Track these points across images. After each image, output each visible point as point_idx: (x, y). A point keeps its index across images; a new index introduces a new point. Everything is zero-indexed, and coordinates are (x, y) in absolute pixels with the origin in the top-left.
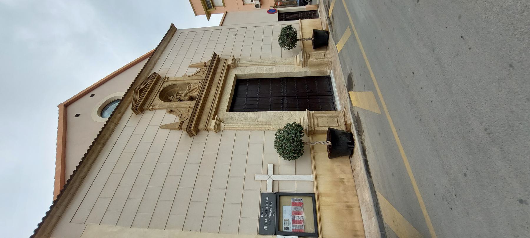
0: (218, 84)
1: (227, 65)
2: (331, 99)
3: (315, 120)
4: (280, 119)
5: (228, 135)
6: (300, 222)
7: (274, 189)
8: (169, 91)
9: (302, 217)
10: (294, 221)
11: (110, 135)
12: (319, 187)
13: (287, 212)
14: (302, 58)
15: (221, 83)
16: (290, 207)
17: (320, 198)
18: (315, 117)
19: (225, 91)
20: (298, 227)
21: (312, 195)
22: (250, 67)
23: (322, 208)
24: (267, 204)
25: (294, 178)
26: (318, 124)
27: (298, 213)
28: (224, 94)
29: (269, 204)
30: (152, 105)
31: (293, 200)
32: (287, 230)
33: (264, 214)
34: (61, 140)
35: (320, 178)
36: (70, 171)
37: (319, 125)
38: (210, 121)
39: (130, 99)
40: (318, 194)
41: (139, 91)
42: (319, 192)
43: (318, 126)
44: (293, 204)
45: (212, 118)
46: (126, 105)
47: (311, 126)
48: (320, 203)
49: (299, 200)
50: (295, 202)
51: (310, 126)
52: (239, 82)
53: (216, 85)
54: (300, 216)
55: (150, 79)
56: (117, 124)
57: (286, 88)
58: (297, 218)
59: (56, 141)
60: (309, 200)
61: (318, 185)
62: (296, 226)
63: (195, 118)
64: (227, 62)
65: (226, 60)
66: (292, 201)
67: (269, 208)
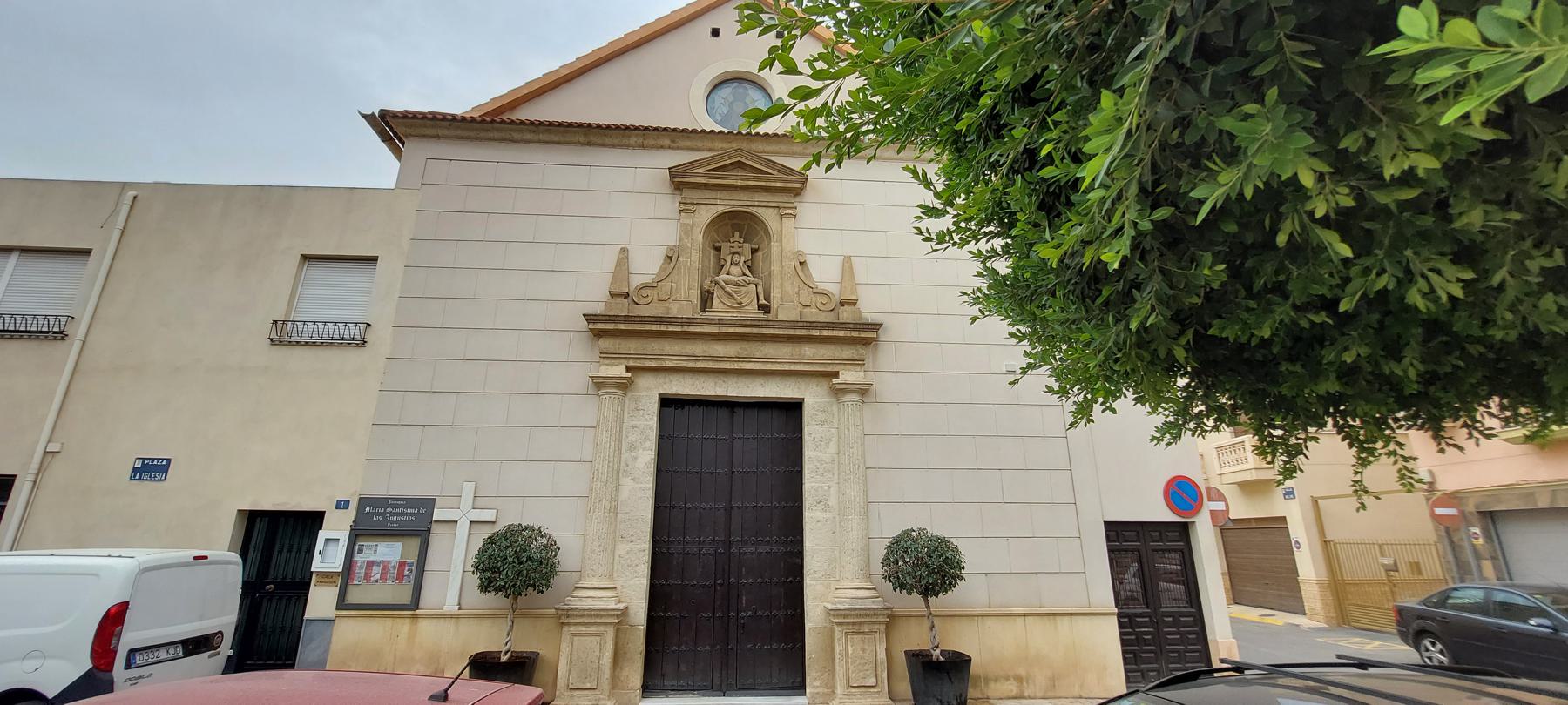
0: (748, 359)
1: (836, 369)
2: (708, 684)
3: (593, 629)
4: (625, 536)
5: (588, 411)
6: (367, 576)
7: (440, 525)
8: (758, 229)
9: (377, 581)
10: (371, 563)
11: (613, 146)
12: (430, 620)
13: (388, 551)
14: (847, 606)
15: (757, 364)
16: (398, 558)
17: (407, 620)
18: (602, 629)
19: (735, 379)
20: (359, 572)
21: (415, 604)
22: (835, 439)
23: (389, 622)
24: (412, 511)
25: (456, 567)
26: (581, 635)
27: (384, 576)
28: (725, 379)
29: (410, 514)
30: (692, 207)
31: (411, 564)
32: (359, 549)
33: (393, 506)
34: (566, 72)
35: (449, 626)
36: (505, 117)
37: (576, 638)
38: (622, 361)
39: (719, 145)
40: (415, 617)
41: (739, 159)
42: (420, 620)
43: (574, 635)
44: (402, 564)
45: (631, 363)
46: (699, 144)
47: (573, 615)
48: (398, 620)
49: (408, 576)
50: (407, 568)
51: (570, 613)
52: (794, 409)
53: (746, 353)
54: (378, 576)
55: (780, 171)
56: (643, 147)
57: (760, 550)
58: (376, 570)
59: (588, 51)
60: (403, 594)
61: (435, 620)
62: (394, 567)
63: (622, 327)
64: (843, 367)
65: (858, 363)
66: (409, 561)
67: (403, 514)
